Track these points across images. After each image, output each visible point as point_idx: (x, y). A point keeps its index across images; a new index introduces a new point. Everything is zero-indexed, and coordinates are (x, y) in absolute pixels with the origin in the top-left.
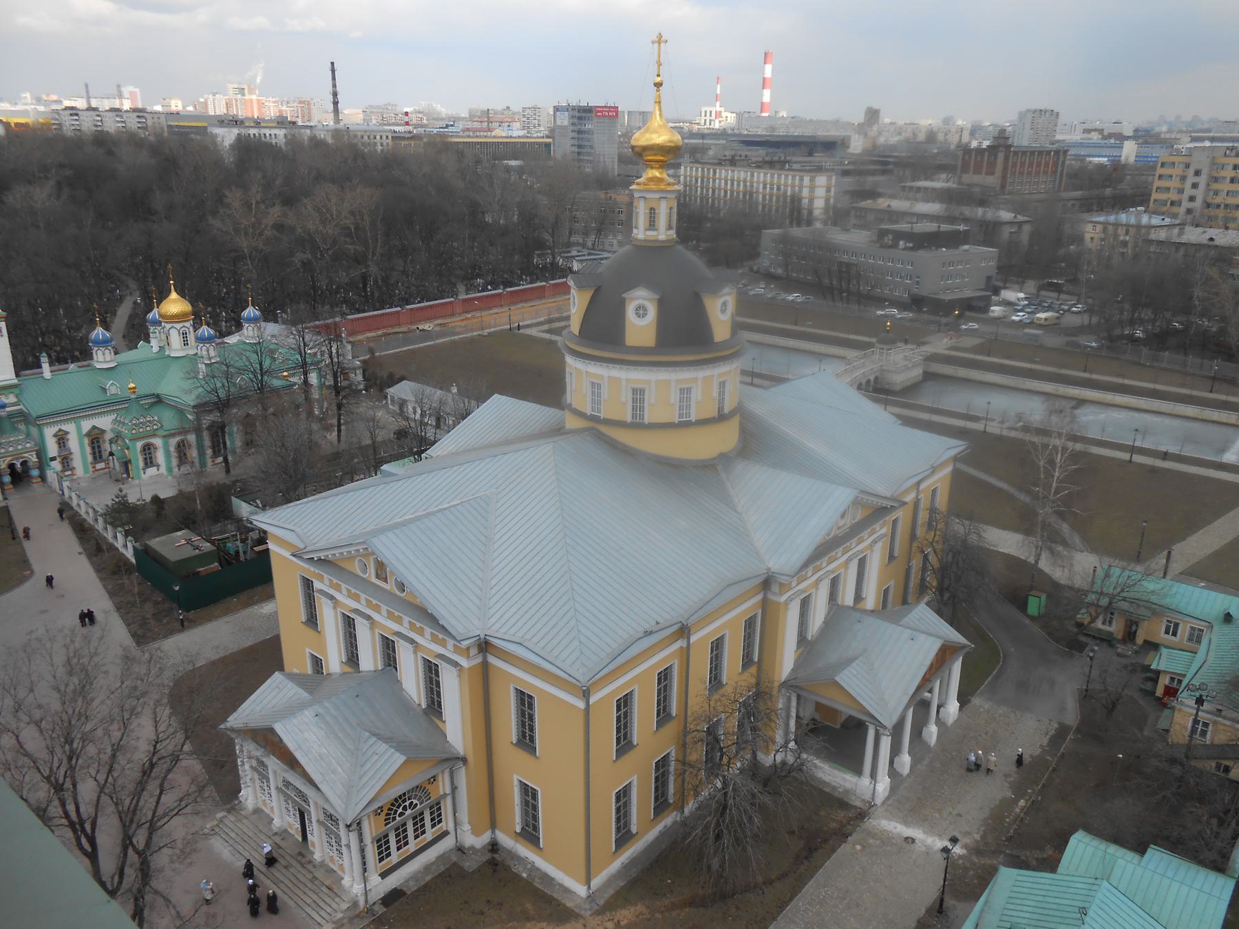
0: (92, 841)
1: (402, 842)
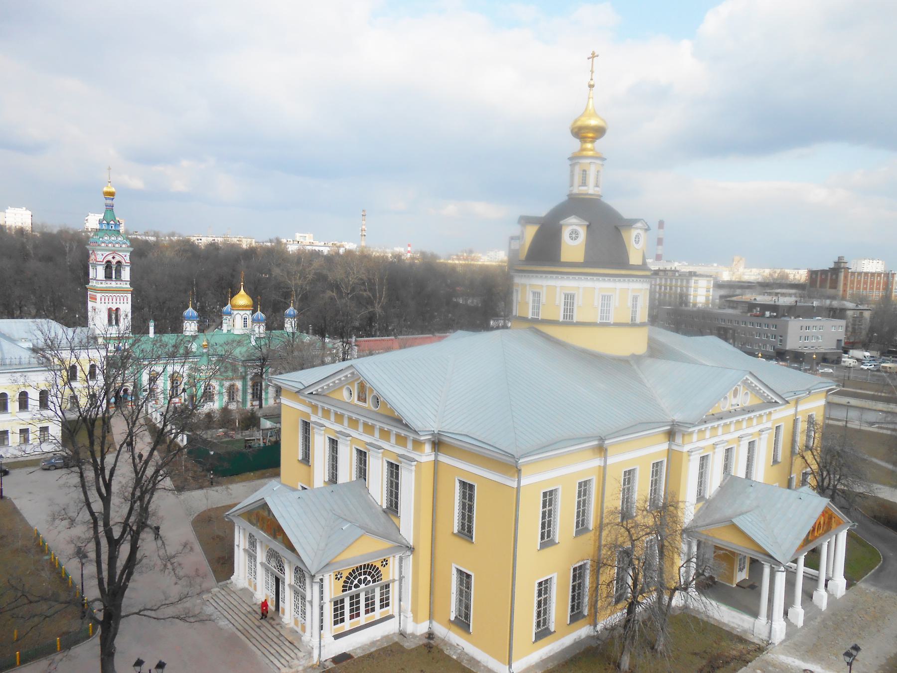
0: (108, 486)
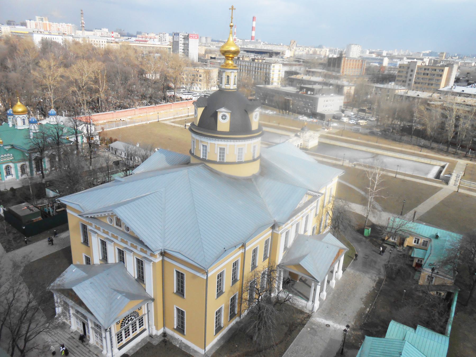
1: (127, 334)
